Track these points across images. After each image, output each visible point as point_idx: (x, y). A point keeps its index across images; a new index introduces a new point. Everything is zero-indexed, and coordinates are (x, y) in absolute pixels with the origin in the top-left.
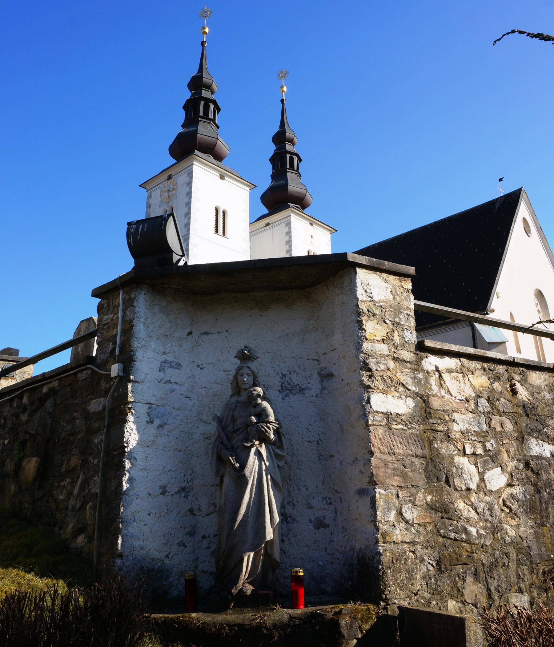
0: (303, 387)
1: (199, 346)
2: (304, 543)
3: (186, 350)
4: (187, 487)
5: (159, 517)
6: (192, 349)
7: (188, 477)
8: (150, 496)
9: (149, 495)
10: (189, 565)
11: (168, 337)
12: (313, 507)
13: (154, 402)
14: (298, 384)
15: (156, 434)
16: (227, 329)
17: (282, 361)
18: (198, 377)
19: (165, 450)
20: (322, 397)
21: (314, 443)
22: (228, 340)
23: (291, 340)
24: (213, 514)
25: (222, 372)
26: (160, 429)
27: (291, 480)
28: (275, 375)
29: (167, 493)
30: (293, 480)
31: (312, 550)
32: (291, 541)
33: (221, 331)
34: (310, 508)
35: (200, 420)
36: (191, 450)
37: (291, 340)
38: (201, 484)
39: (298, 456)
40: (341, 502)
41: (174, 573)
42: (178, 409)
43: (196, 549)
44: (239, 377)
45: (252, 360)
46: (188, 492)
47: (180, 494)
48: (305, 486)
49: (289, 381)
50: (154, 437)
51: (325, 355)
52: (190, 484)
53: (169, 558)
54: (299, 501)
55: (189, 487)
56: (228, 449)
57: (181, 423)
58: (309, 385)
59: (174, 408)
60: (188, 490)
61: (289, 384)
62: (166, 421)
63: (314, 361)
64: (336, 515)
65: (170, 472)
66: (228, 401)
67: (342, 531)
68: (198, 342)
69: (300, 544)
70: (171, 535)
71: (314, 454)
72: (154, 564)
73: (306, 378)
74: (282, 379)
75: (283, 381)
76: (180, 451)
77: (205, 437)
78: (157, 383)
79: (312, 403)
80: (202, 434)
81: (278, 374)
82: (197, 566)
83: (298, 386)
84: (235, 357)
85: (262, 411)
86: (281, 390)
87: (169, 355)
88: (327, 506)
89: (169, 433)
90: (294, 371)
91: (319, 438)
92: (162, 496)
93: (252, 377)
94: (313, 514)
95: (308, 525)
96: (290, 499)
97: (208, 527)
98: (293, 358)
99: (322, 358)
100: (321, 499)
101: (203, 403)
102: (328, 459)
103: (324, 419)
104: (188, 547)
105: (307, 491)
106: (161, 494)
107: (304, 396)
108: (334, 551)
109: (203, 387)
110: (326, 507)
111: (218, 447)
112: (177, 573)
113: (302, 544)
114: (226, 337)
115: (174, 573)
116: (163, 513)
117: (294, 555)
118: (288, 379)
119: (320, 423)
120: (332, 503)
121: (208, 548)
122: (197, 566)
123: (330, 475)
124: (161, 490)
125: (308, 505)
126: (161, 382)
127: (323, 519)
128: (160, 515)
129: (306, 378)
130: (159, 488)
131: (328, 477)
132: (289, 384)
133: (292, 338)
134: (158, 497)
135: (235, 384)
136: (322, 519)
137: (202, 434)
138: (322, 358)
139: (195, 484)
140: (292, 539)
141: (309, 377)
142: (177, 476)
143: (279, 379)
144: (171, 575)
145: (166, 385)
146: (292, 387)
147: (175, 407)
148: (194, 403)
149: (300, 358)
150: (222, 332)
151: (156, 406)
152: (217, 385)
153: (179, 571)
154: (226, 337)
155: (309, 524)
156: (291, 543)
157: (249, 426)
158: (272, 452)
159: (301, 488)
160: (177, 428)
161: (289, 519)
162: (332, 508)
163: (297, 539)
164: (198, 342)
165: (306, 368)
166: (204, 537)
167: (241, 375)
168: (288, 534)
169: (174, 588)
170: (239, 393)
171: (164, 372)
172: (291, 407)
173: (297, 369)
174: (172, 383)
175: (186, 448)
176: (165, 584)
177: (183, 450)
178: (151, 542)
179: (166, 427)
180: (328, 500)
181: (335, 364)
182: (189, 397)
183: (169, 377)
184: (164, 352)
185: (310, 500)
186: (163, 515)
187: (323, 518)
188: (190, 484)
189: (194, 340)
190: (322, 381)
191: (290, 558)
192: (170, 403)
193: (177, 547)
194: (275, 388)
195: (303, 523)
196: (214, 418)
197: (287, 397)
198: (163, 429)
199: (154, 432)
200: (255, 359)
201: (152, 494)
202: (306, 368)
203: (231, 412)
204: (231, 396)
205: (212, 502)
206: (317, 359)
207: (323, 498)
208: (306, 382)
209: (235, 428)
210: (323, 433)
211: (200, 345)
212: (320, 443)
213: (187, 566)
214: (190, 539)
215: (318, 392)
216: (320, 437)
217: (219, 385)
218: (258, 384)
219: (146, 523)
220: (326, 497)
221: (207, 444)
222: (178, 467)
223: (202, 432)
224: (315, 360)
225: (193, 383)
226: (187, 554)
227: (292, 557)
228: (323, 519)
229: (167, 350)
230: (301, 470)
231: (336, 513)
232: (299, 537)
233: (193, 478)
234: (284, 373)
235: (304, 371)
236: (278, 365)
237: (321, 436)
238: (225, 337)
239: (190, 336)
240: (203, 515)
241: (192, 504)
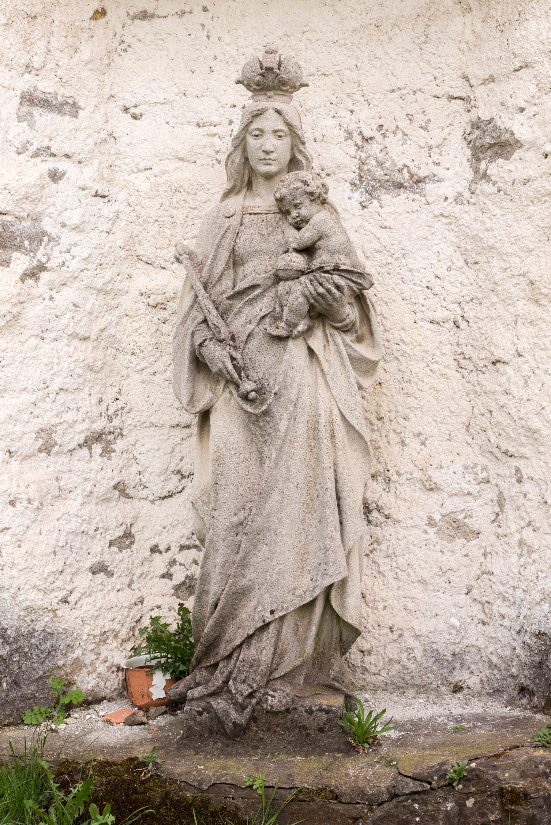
0: (422, 173)
1: (125, 51)
2: (413, 574)
3: (90, 62)
4: (107, 430)
5: (38, 509)
6: (106, 61)
7: (108, 406)
8: (11, 457)
9: (8, 454)
10: (120, 617)
11: (39, 20)
12: (438, 489)
13: (8, 209)
14: (405, 166)
15: (19, 294)
16: (205, 5)
17: (362, 99)
18: (126, 139)
19: (45, 336)
20: (474, 204)
21: (447, 325)
22: (208, 37)
23: (390, 39)
24: (177, 495)
25: (192, 129)
26: (30, 282)
27: (380, 419)
28: (342, 139)
29: (56, 448)
30: (386, 419)
31: (434, 591)
32: (379, 567)
33: (187, 9)
34: (431, 490)
35: (135, 258)
36: (114, 336)
37: (390, 39)
38: (144, 422)
39: (400, 358)
40: (519, 481)
41: (85, 637)
42: (76, 228)
43: (135, 578)
44: (250, 140)
45: (287, 91)
46: (109, 443)
47: (90, 448)
48: (419, 434)
49: (381, 156)
50: (15, 305)
51: (492, 85)
52: (116, 422)
53: (72, 604)
54: (402, 472)
55: (112, 430)
56: (221, 341)
57: (85, 267)
58: (437, 170)
59: (64, 225)
60: (110, 437)
61: (380, 164)
62: (44, 260)
63: (453, 101)
64: (502, 510)
65: (62, 395)
66: (219, 209)
67: (519, 551)
68: (123, 41)
69: (403, 576)
70: (71, 551)
71: (444, 354)
72: (32, 621)
73: (431, 148)
74: (362, 151)
75: (363, 155)
76: (85, 339)
77: (151, 303)
78: (15, 156)
79: (444, 220)
80: (142, 295)
81: (349, 135)
82: (141, 617)
83: (405, 171)
84: (238, 82)
85: (319, 239)
86: (357, 182)
87: (42, 73)
88: (478, 487)
89: (54, 293)
90: (394, 129)
91: (460, 312)
92: (43, 455)
93: (287, 141)
94: (439, 504)
95: (426, 532)
96: (380, 468)
97: (164, 528)
98: (393, 91)
99: (480, 92)
100: (459, 470)
101: (143, 213)
102: (484, 369)
103: (476, 263)
104: (115, 576)
105: (422, 447)
106: (40, 450)
107: (423, 199)
108: (492, 597)
109: (141, 167)
110: (474, 488)
111: (193, 334)
112: (91, 637)
113: (409, 575)
114: (203, 26)
115: (85, 637)
116: (50, 497)
117: (386, 601)
118: (378, 151)
119: (463, 273)
120: (491, 480)
121: (167, 576)
122: (141, 617)
123: (491, 412)
124: (40, 442)
125: (427, 484)
126: (24, 152)
127: (465, 518)
128: (41, 504)
129: (431, 148)
130: (33, 435)
131: (483, 415)
132: (380, 164)
133: (391, 35)
134: (34, 458)
135: (237, 160)
136: (460, 517)
137: (142, 295)
138: (480, 92)
139: (129, 422)
140: (381, 564)
141: (437, 147)
142: (80, 404)
143: (352, 150)
144: (77, 644)
145: (38, 160)
146: (388, 173)
147: (67, 223)
148: (118, 212)
149: (415, 92)
150: (191, 13)
151: (14, 219)
152: (180, 164)
153: (97, 632)
154: (203, 26)
155: (427, 528)
156: (380, 572)
157: (281, 280)
158: (344, 353)
159: (407, 441)
160: (75, 278)
161: (375, 514)
162: (490, 493)
163: (395, 565)
164: (123, 41)
165: (429, 120)
166: (155, 550)
167: (257, 136)
168: (371, 552)
169: (85, 671)
170: (249, 185)
171: (32, 126)
172: (386, 228)
173: (404, 124)
174: (55, 155)
175: (102, 330)
176: (64, 665)
177: (95, 337)
178: (21, 570)
179: (45, 276)
180: (479, 472)
181: (522, 110)
182: (104, 197)
183: (47, 139)
184: (27, 67)
185: (431, 472)
186: (49, 502)
187: (463, 515)
188: (116, 422)
189: (111, 35)
190: (476, 158)
191: (377, 609)
192: (52, 209)
193: (90, 578)
194: (341, 175)
195: (412, 526)
196: (181, 255)
197: (375, 202)
198: (37, 280)
199: (14, 290)
200: (295, 88)
201: (16, 452)
202: (429, 120)
203: (228, 241)
204: (227, 194)
205: (173, 467)
206: (463, 95)
207: (466, 468)
208: (430, 161)
209: (241, 286)
210: (472, 300)
211: (129, 49)
212: (463, 325)
213: (117, 620)
214: (120, 556)
215: (461, 189)
216: (462, 309)
217: (186, 164)
218: (304, 161)
219: (7, 526)
220: (476, 465)
221: (156, 321)
222: (81, 380)
223: (143, 291)
224: (455, 98)
225: (114, 158)
226: (115, 591)
227: (381, 606)
228: (465, 518)
229: (36, 59)
230: (408, 395)
231: (501, 505)
232: (400, 560)
233: (122, 408)
234: (368, 133)
235: (425, 128)
236: (352, 112)
237: (466, 309)
238: (201, 27)
239: (102, 21)
240: (151, 498)
241: (123, 471)
